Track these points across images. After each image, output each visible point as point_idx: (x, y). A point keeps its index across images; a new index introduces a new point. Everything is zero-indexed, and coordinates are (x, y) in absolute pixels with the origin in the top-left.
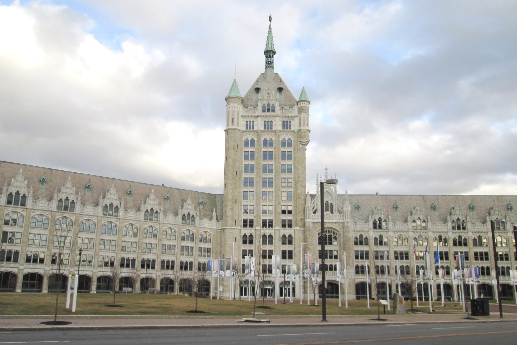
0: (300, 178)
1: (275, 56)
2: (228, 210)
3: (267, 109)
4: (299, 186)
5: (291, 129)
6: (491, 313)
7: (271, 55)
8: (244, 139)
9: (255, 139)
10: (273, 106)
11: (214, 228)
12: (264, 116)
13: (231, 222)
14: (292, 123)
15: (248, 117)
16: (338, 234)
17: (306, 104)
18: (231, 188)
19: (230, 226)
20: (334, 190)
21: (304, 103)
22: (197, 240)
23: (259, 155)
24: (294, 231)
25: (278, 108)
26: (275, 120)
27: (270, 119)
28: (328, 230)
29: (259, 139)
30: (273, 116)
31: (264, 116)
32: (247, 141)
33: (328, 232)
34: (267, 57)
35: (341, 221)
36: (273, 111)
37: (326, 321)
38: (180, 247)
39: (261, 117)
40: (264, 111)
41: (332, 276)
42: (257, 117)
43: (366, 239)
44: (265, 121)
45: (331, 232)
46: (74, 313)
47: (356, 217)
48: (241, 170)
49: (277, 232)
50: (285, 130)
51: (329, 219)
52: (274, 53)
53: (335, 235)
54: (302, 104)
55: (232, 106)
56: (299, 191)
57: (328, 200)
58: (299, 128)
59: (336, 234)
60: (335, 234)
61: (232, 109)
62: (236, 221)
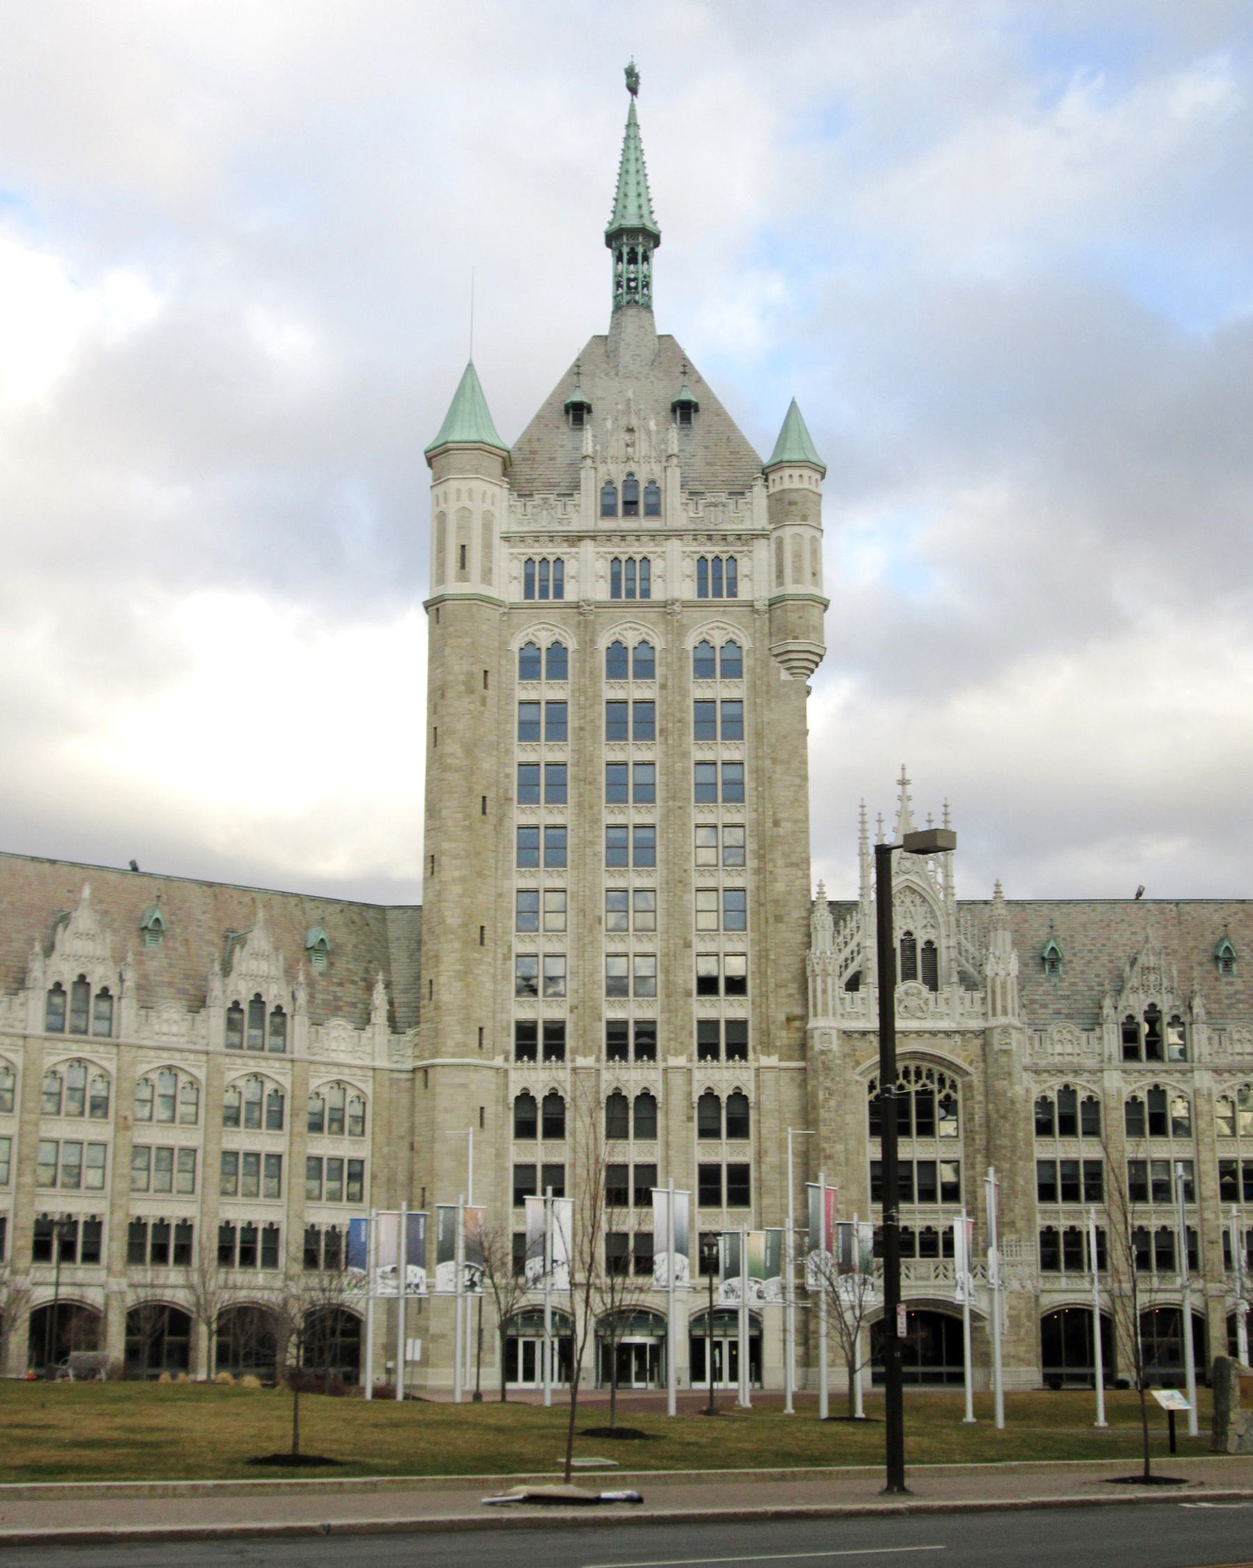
0: (783, 824)
1: (657, 255)
2: (443, 979)
3: (626, 503)
4: (780, 862)
5: (735, 595)
8: (516, 644)
9: (571, 643)
10: (654, 490)
11: (378, 1064)
12: (609, 536)
13: (459, 1037)
15: (537, 539)
16: (959, 1086)
18: (457, 874)
19: (454, 1055)
20: (940, 878)
21: (796, 472)
22: (295, 1123)
24: (757, 1076)
25: (673, 499)
26: (662, 556)
28: (912, 1069)
29: (588, 644)
30: (654, 536)
31: (609, 536)
33: (913, 1078)
35: (976, 1024)
36: (654, 510)
37: (903, 1490)
39: (593, 538)
40: (608, 511)
41: (932, 1282)
42: (576, 539)
43: (1092, 1105)
44: (616, 559)
45: (930, 1076)
47: (1044, 1006)
48: (506, 790)
49: (677, 1080)
51: (919, 1014)
53: (947, 1090)
56: (780, 887)
57: (912, 928)
58: (776, 592)
59: (953, 1086)
60: (948, 1083)
61: (460, 505)
62: (481, 1029)
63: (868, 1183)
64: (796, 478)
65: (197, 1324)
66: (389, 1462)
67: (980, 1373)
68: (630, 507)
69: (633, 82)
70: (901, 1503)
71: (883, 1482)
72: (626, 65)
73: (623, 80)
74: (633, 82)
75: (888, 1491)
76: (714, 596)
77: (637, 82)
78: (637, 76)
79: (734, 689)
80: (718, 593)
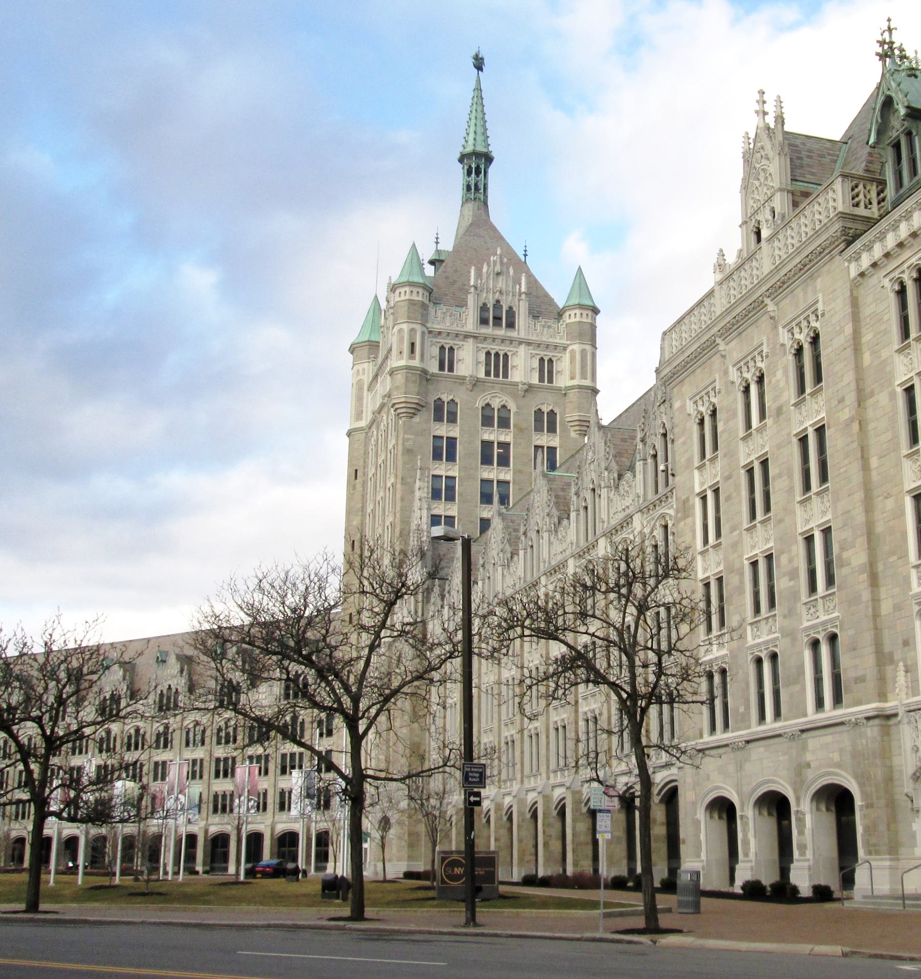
1: (492, 170)
3: (494, 318)
5: (552, 382)
6: (492, 848)
7: (482, 167)
10: (511, 313)
14: (458, 354)
17: (584, 315)
23: (469, 449)
25: (522, 319)
27: (502, 349)
32: (439, 403)
34: (469, 173)
36: (511, 325)
37: (476, 925)
38: (167, 650)
39: (475, 337)
40: (484, 321)
46: (162, 880)
50: (446, 372)
52: (489, 159)
54: (573, 316)
55: (570, 315)
63: (91, 641)
64: (415, 293)
65: (327, 875)
66: (178, 906)
67: (195, 769)
68: (497, 320)
69: (479, 64)
70: (471, 930)
71: (462, 919)
72: (473, 54)
73: (470, 62)
74: (479, 64)
75: (467, 924)
76: (494, 376)
77: (483, 63)
78: (482, 59)
79: (507, 436)
80: (497, 375)
